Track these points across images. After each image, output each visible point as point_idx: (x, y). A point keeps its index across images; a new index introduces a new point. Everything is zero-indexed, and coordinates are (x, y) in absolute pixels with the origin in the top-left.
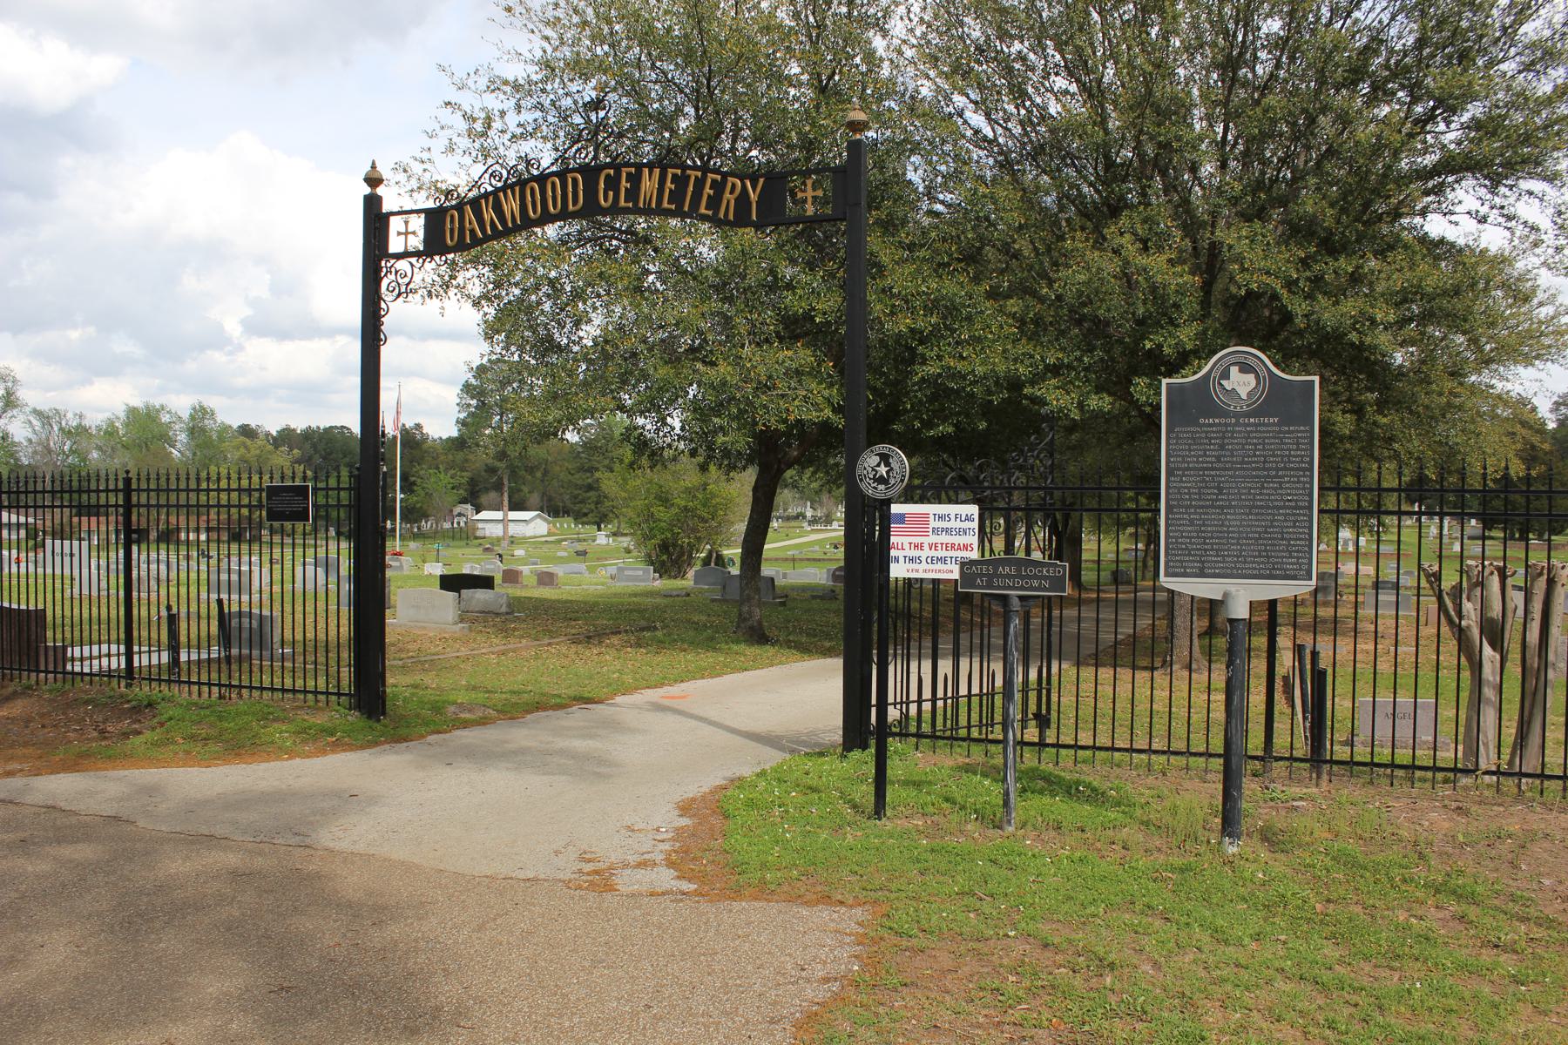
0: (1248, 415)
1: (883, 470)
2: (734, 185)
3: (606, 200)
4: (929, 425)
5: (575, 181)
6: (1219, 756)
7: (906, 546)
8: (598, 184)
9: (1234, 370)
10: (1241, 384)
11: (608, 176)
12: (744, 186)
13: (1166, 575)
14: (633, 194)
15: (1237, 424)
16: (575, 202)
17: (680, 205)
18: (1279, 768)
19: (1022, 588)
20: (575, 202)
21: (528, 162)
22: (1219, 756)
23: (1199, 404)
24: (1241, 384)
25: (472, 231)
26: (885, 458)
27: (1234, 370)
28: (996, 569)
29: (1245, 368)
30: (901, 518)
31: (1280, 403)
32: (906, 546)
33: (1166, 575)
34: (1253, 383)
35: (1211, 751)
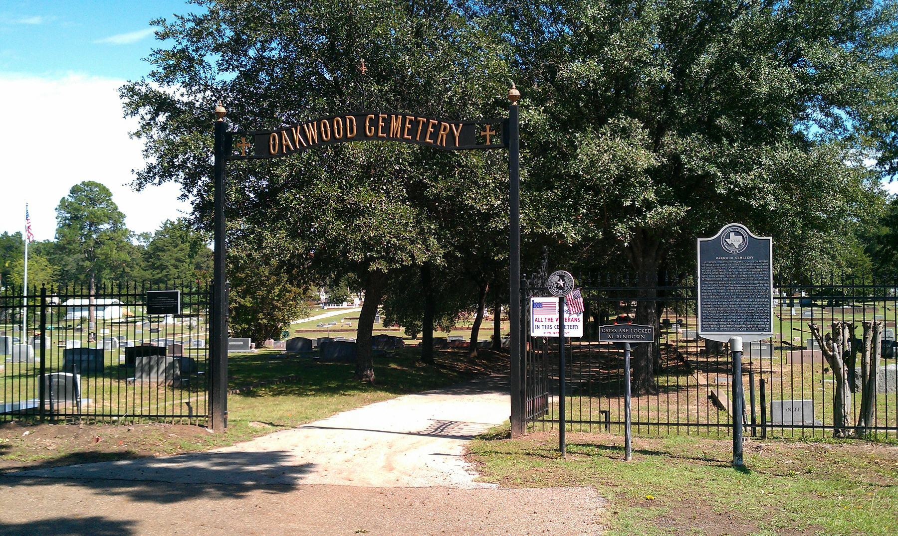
0: (739, 255)
1: (561, 283)
2: (445, 128)
3: (370, 132)
4: (497, 255)
5: (351, 120)
6: (557, 421)
7: (544, 320)
8: (365, 122)
9: (732, 234)
10: (736, 241)
11: (371, 119)
12: (451, 127)
13: (702, 331)
14: (386, 129)
15: (734, 259)
16: (352, 132)
17: (414, 137)
18: (613, 427)
19: (632, 339)
20: (352, 132)
21: (132, 90)
22: (557, 421)
23: (715, 250)
24: (736, 241)
25: (287, 146)
26: (562, 277)
27: (732, 234)
28: (618, 330)
29: (737, 233)
30: (540, 305)
31: (753, 249)
32: (544, 320)
33: (702, 331)
34: (741, 240)
35: (573, 419)
